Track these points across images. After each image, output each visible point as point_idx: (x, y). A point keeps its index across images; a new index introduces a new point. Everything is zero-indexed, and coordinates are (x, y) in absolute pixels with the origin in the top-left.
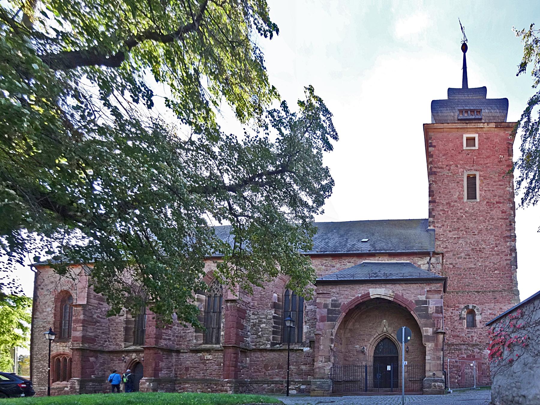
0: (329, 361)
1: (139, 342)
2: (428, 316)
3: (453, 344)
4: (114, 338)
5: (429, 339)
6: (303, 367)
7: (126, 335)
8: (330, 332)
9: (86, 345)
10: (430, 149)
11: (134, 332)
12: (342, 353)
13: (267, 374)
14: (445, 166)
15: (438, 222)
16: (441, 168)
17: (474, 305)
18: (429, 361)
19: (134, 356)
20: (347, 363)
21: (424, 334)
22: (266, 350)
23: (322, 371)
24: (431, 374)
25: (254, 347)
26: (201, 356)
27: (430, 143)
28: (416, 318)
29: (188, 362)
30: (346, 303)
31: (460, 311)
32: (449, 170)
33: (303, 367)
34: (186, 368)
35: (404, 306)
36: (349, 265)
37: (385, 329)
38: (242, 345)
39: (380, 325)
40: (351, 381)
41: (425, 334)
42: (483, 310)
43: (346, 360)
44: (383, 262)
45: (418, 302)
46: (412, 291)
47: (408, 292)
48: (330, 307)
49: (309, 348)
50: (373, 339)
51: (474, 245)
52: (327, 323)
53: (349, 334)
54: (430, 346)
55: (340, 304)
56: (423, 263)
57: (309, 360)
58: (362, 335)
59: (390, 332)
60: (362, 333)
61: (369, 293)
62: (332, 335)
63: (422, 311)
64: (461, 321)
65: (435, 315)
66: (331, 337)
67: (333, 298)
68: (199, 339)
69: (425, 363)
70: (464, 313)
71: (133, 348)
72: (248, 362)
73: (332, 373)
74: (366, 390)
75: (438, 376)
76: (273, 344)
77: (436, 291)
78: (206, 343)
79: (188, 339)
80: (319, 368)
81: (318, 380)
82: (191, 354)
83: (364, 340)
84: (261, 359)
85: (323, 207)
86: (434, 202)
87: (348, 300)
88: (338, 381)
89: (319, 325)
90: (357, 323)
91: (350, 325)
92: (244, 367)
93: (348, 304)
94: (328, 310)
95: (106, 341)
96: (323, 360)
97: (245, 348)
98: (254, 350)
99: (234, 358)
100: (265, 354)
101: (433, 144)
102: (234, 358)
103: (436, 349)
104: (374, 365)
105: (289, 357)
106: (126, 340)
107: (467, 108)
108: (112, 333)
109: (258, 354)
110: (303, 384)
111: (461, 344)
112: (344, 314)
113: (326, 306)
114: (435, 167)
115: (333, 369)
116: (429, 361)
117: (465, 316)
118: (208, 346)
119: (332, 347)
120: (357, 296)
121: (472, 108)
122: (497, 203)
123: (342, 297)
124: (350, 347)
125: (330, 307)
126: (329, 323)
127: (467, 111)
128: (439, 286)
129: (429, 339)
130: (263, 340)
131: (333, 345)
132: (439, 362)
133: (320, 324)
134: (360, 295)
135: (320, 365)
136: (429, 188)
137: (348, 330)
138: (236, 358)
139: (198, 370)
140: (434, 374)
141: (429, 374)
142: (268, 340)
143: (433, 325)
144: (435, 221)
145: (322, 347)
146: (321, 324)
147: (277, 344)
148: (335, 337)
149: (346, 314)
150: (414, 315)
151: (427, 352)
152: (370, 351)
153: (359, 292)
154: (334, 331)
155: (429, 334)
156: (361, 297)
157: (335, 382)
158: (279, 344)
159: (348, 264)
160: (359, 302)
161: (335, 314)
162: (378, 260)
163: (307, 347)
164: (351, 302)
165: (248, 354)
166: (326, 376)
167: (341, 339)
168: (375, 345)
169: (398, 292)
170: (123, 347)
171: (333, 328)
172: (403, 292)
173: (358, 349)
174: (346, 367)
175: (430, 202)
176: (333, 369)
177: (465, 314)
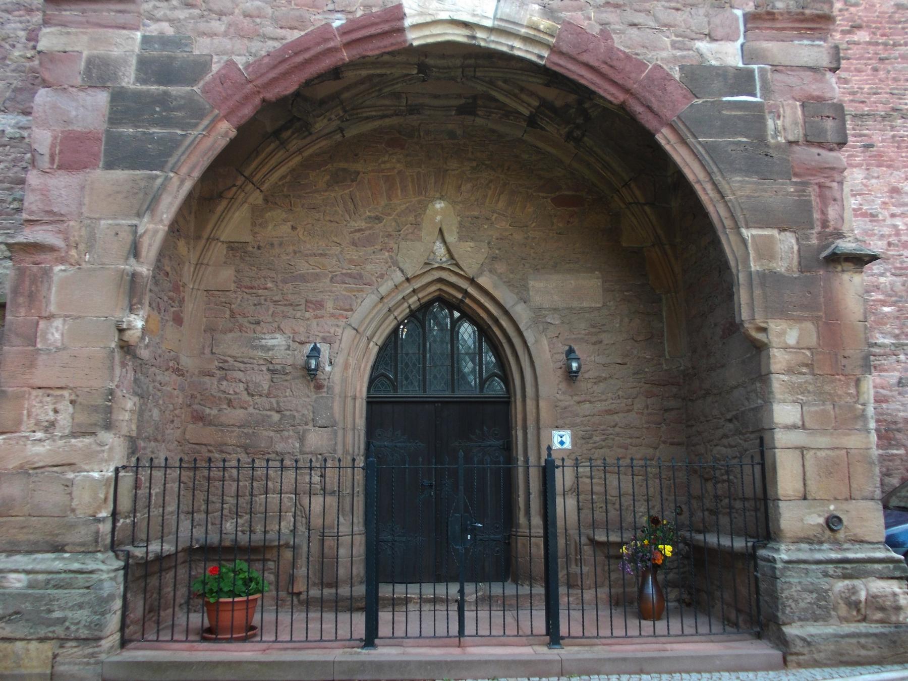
0: (108, 426)
12: (179, 372)
24: (817, 520)
30: (240, 61)
39: (417, 225)
40: (235, 550)
41: (754, 267)
43: (199, 418)
46: (665, 16)
47: (640, 18)
48: (129, 80)
54: (792, 337)
55: (203, 65)
58: (303, 278)
59: (470, 266)
60: (303, 267)
62: (135, 251)
63: (728, 126)
66: (134, 265)
67: (154, 29)
73: (125, 503)
75: (860, 531)
83: (320, 305)
89: (44, 193)
90: (278, 214)
94: (118, 96)
96: (64, 420)
112: (225, 130)
119: (132, 336)
120: (317, 20)
123: (218, 26)
125: (129, 80)
126: (120, 174)
134: (338, 22)
140: (833, 523)
148: (158, 266)
149: (241, 129)
155: (781, 266)
156: (344, 31)
161: (164, 122)
164: (279, 59)
166: (82, 534)
168: (380, 338)
169: (577, 17)
171: (151, 205)
172: (611, 16)
176: (127, 477)
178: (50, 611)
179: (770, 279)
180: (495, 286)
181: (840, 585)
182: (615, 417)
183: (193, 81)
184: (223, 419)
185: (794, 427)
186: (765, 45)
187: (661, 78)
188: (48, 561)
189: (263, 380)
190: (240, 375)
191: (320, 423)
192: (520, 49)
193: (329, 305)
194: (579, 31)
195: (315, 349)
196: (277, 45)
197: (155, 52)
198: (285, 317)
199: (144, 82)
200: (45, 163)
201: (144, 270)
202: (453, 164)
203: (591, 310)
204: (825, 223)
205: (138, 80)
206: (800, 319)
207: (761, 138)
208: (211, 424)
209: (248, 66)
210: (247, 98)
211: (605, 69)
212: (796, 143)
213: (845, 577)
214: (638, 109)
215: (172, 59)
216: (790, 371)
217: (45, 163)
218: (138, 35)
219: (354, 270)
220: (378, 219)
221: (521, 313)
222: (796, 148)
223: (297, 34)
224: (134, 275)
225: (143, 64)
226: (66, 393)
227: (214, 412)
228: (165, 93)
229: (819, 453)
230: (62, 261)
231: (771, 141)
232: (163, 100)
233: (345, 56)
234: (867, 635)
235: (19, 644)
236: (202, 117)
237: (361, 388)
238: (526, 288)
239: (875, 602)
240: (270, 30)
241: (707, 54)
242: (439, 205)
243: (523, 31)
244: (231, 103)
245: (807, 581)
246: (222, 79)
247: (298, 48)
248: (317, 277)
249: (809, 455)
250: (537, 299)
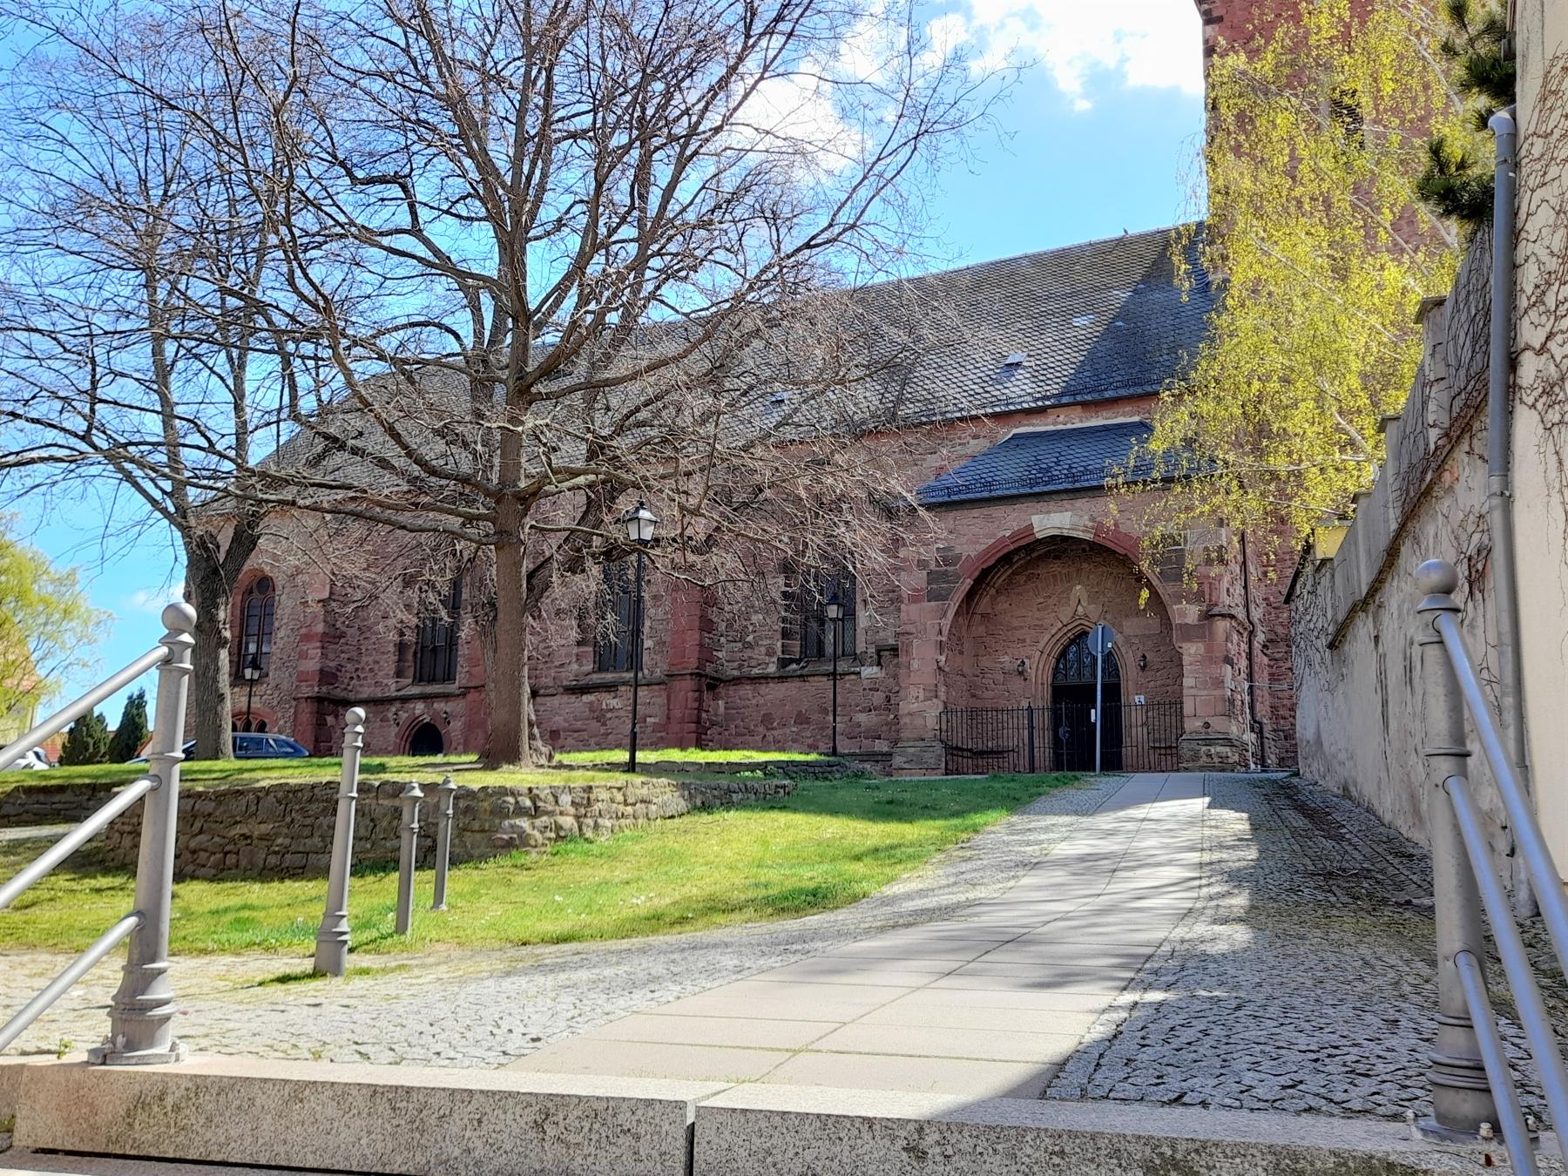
1: (426, 678)
4: (371, 670)
5: (1189, 633)
6: (862, 718)
7: (399, 660)
9: (324, 689)
11: (415, 653)
13: (771, 739)
18: (1193, 692)
19: (420, 707)
20: (978, 704)
21: (1177, 621)
22: (765, 678)
23: (919, 721)
24: (1199, 724)
25: (736, 673)
26: (591, 703)
29: (557, 718)
33: (862, 718)
34: (552, 732)
36: (976, 446)
37: (1080, 609)
38: (709, 669)
43: (973, 696)
44: (1069, 426)
48: (933, 566)
49: (875, 669)
50: (1047, 637)
52: (926, 604)
54: (1192, 651)
55: (959, 557)
57: (878, 699)
60: (1015, 623)
62: (940, 633)
66: (939, 638)
68: (585, 662)
71: (416, 690)
72: (722, 710)
73: (944, 727)
76: (784, 663)
78: (600, 670)
79: (557, 664)
80: (910, 714)
81: (911, 744)
82: (565, 698)
83: (1024, 641)
84: (754, 702)
88: (957, 748)
90: (1003, 598)
91: (984, 605)
92: (713, 724)
93: (978, 557)
95: (352, 678)
96: (921, 697)
97: (715, 675)
98: (736, 681)
99: (696, 700)
100: (763, 689)
102: (696, 700)
103: (1209, 659)
106: (399, 674)
108: (364, 659)
109: (747, 690)
112: (969, 582)
113: (922, 564)
115: (944, 717)
116: (1193, 692)
118: (609, 677)
119: (941, 664)
120: (1000, 535)
124: (985, 662)
125: (933, 566)
126: (933, 603)
130: (759, 653)
131: (943, 658)
132: (1217, 693)
133: (910, 611)
135: (914, 707)
137: (978, 617)
138: (700, 700)
139: (585, 735)
140: (1207, 725)
141: (1192, 725)
142: (770, 653)
143: (1199, 597)
145: (915, 665)
146: (914, 607)
147: (792, 661)
152: (1040, 671)
153: (1006, 524)
154: (947, 623)
157: (952, 748)
158: (798, 661)
159: (973, 442)
160: (1005, 551)
161: (948, 582)
162: (1055, 424)
163: (871, 665)
164: (986, 551)
165: (721, 690)
167: (959, 639)
170: (393, 687)
173: (1008, 666)
174: (973, 713)
179: (1185, 628)
181: (1204, 748)
189: (1001, 678)
192: (1081, 535)
195: (1023, 662)
196: (986, 546)
200: (906, 601)
202: (1085, 565)
203: (1154, 635)
217: (906, 601)
219: (1037, 622)
233: (1012, 547)
238: (1121, 626)
242: (1078, 587)
248: (1022, 627)
249: (1198, 699)
250: (1127, 631)
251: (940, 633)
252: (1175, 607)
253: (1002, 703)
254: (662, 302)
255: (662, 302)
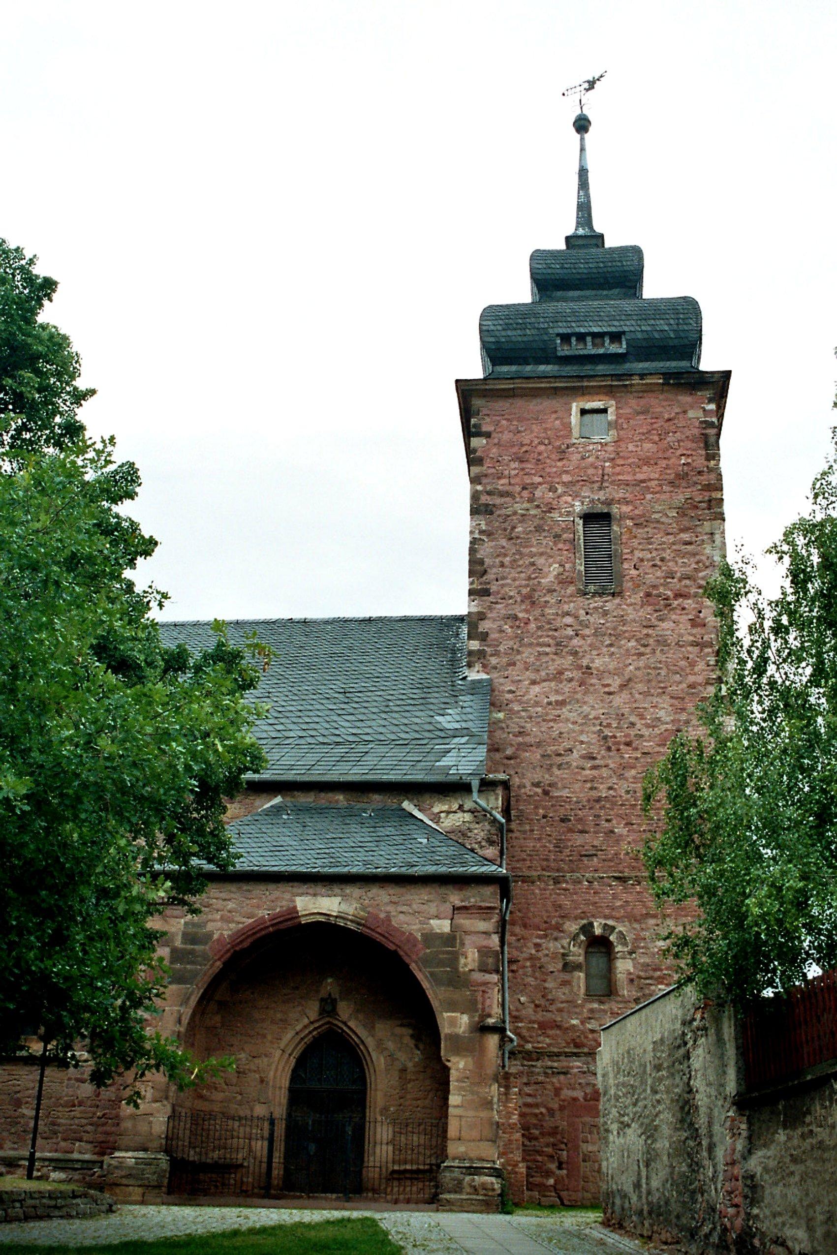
2: (457, 980)
3: (539, 1055)
5: (459, 1045)
8: (176, 1015)
10: (475, 442)
14: (518, 489)
15: (496, 654)
16: (507, 494)
17: (610, 922)
21: (445, 1030)
27: (475, 426)
28: (425, 985)
30: (225, 933)
31: (565, 942)
32: (531, 500)
35: (392, 947)
42: (639, 939)
43: (201, 1097)
45: (430, 938)
48: (178, 943)
50: (290, 1035)
51: (609, 725)
53: (218, 1018)
54: (461, 1065)
55: (210, 935)
56: (445, 808)
61: (295, 907)
62: (179, 1021)
63: (441, 963)
64: (566, 976)
65: (478, 977)
69: (446, 1116)
70: (577, 954)
74: (621, 1226)
77: (481, 908)
83: (264, 1036)
85: (147, 589)
86: (485, 593)
87: (232, 926)
94: (174, 951)
101: (485, 428)
103: (478, 1077)
104: (289, 1115)
105: (41, 1082)
107: (582, 330)
110: (55, 1169)
111: (567, 1055)
114: (489, 493)
117: (581, 959)
121: (596, 330)
122: (678, 595)
123: (218, 916)
125: (178, 943)
127: (581, 337)
128: (488, 895)
129: (459, 1045)
132: (484, 1114)
136: (472, 551)
143: (470, 1007)
144: (488, 650)
149: (224, 964)
150: (420, 976)
151: (453, 1085)
161: (193, 963)
168: (296, 1054)
175: (471, 593)
177: (582, 951)
178: (143, 1174)
179: (454, 1038)
180: (357, 1026)
182: (419, 1102)
183: (206, 944)
184: (213, 1098)
185: (458, 1106)
186: (462, 921)
187: (411, 939)
188: (141, 1154)
190: (222, 1074)
191: (262, 1101)
193: (269, 1037)
194: (376, 917)
196: (241, 926)
197: (190, 930)
198: (246, 1042)
199: (186, 944)
201: (182, 1029)
204: (483, 1009)
205: (182, 943)
206: (465, 1056)
207: (455, 969)
208: (207, 1100)
209: (229, 936)
210: (228, 951)
211: (386, 935)
212: (473, 970)
213: (470, 1174)
214: (402, 953)
215: (196, 933)
216: (457, 1081)
218: (182, 921)
220: (297, 988)
221: (370, 1042)
222: (473, 973)
223: (251, 921)
224: (179, 1032)
225: (185, 934)
226: (150, 1084)
227: (209, 1094)
228: (193, 949)
229: (469, 1119)
230: (150, 1025)
231: (461, 970)
232: (192, 952)
234: (476, 1200)
235: (131, 1188)
236: (209, 961)
237: (285, 1082)
239: (484, 1186)
240: (238, 918)
241: (435, 927)
242: (329, 980)
243: (350, 917)
244: (222, 953)
245: (453, 1175)
246: (218, 940)
247: (251, 927)
251: (179, 1021)
252: (446, 1015)
253: (233, 1109)
254: (584, 210)
255: (584, 210)
